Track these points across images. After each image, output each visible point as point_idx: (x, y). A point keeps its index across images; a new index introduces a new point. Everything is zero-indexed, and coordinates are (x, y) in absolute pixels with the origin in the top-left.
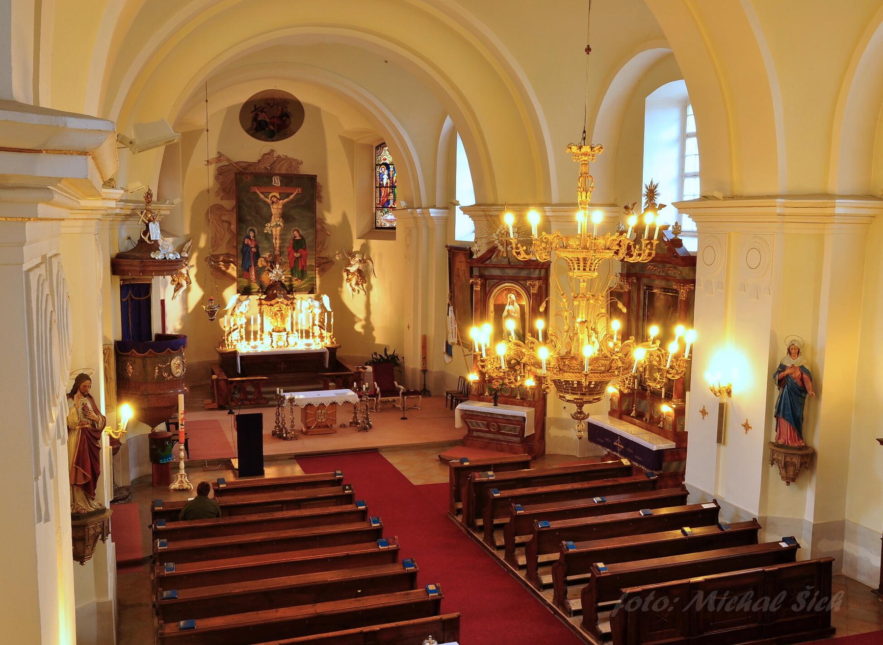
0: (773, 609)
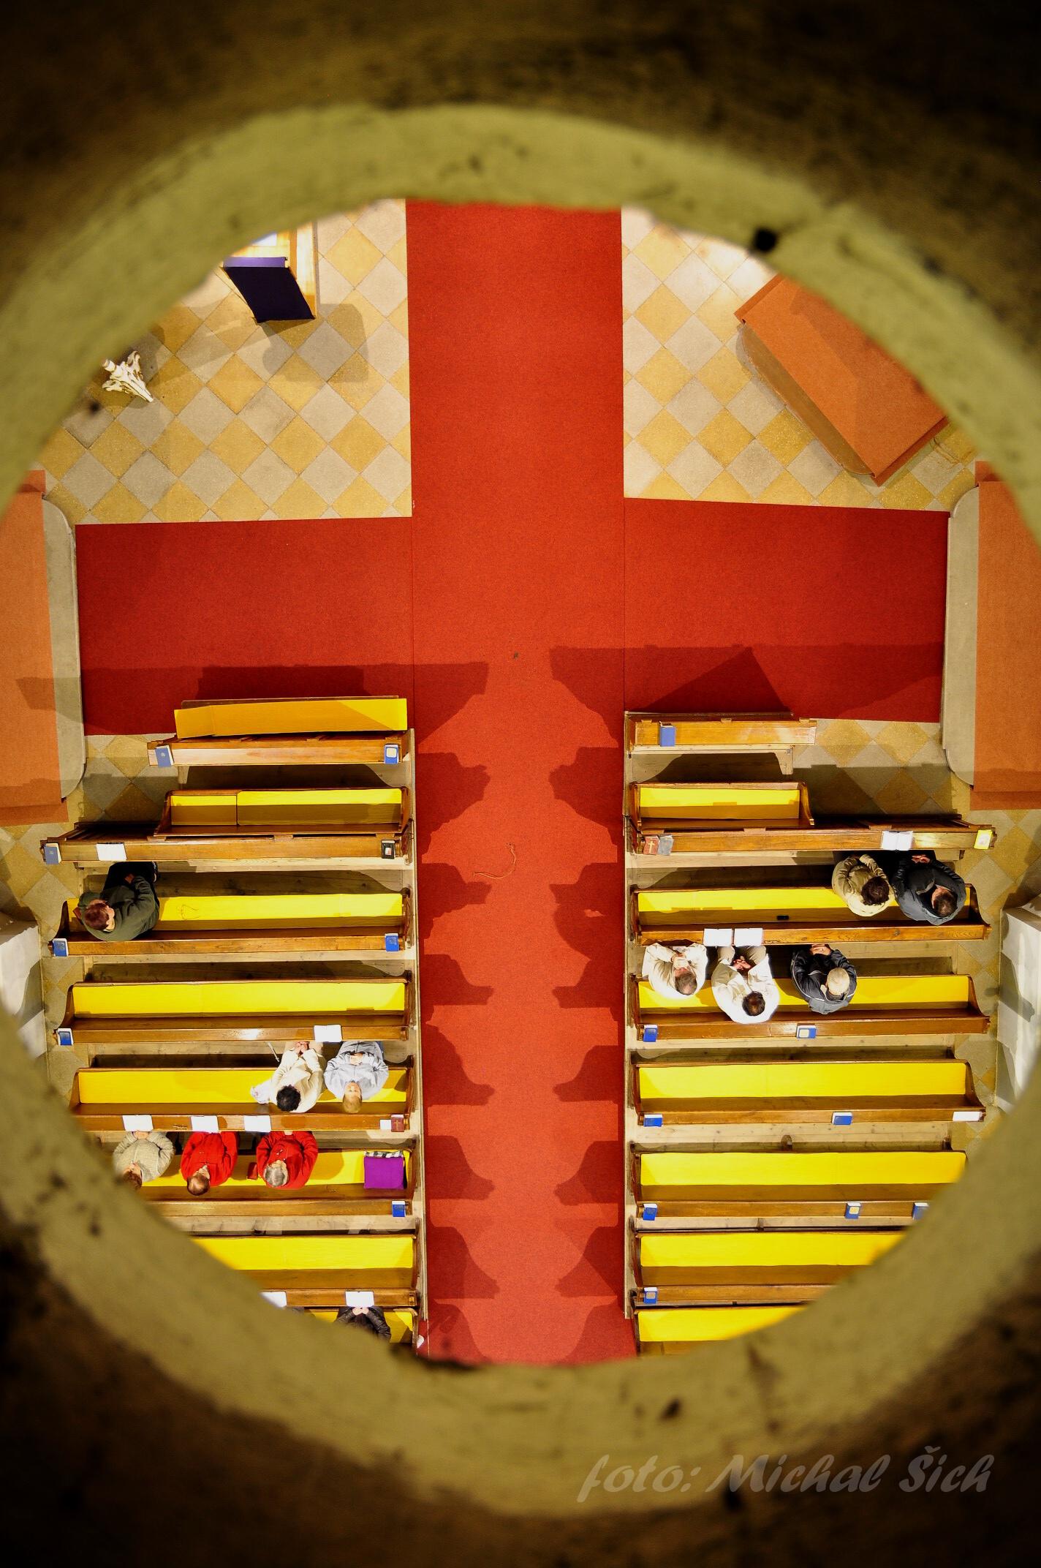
0: (866, 1488)
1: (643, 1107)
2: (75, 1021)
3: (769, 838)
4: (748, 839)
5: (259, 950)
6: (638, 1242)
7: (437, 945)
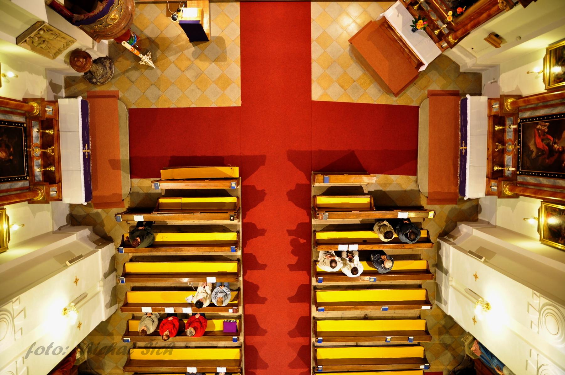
1: (318, 305)
2: (126, 275)
3: (360, 214)
4: (354, 214)
5: (188, 251)
6: (316, 351)
7: (248, 250)
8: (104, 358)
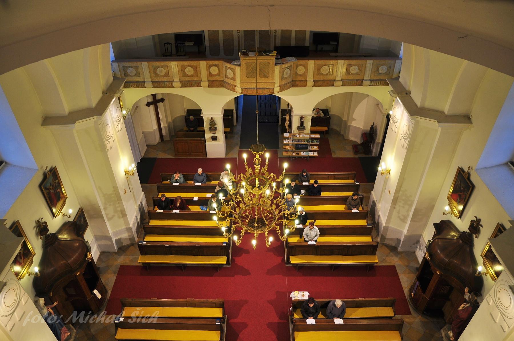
8: (424, 332)
